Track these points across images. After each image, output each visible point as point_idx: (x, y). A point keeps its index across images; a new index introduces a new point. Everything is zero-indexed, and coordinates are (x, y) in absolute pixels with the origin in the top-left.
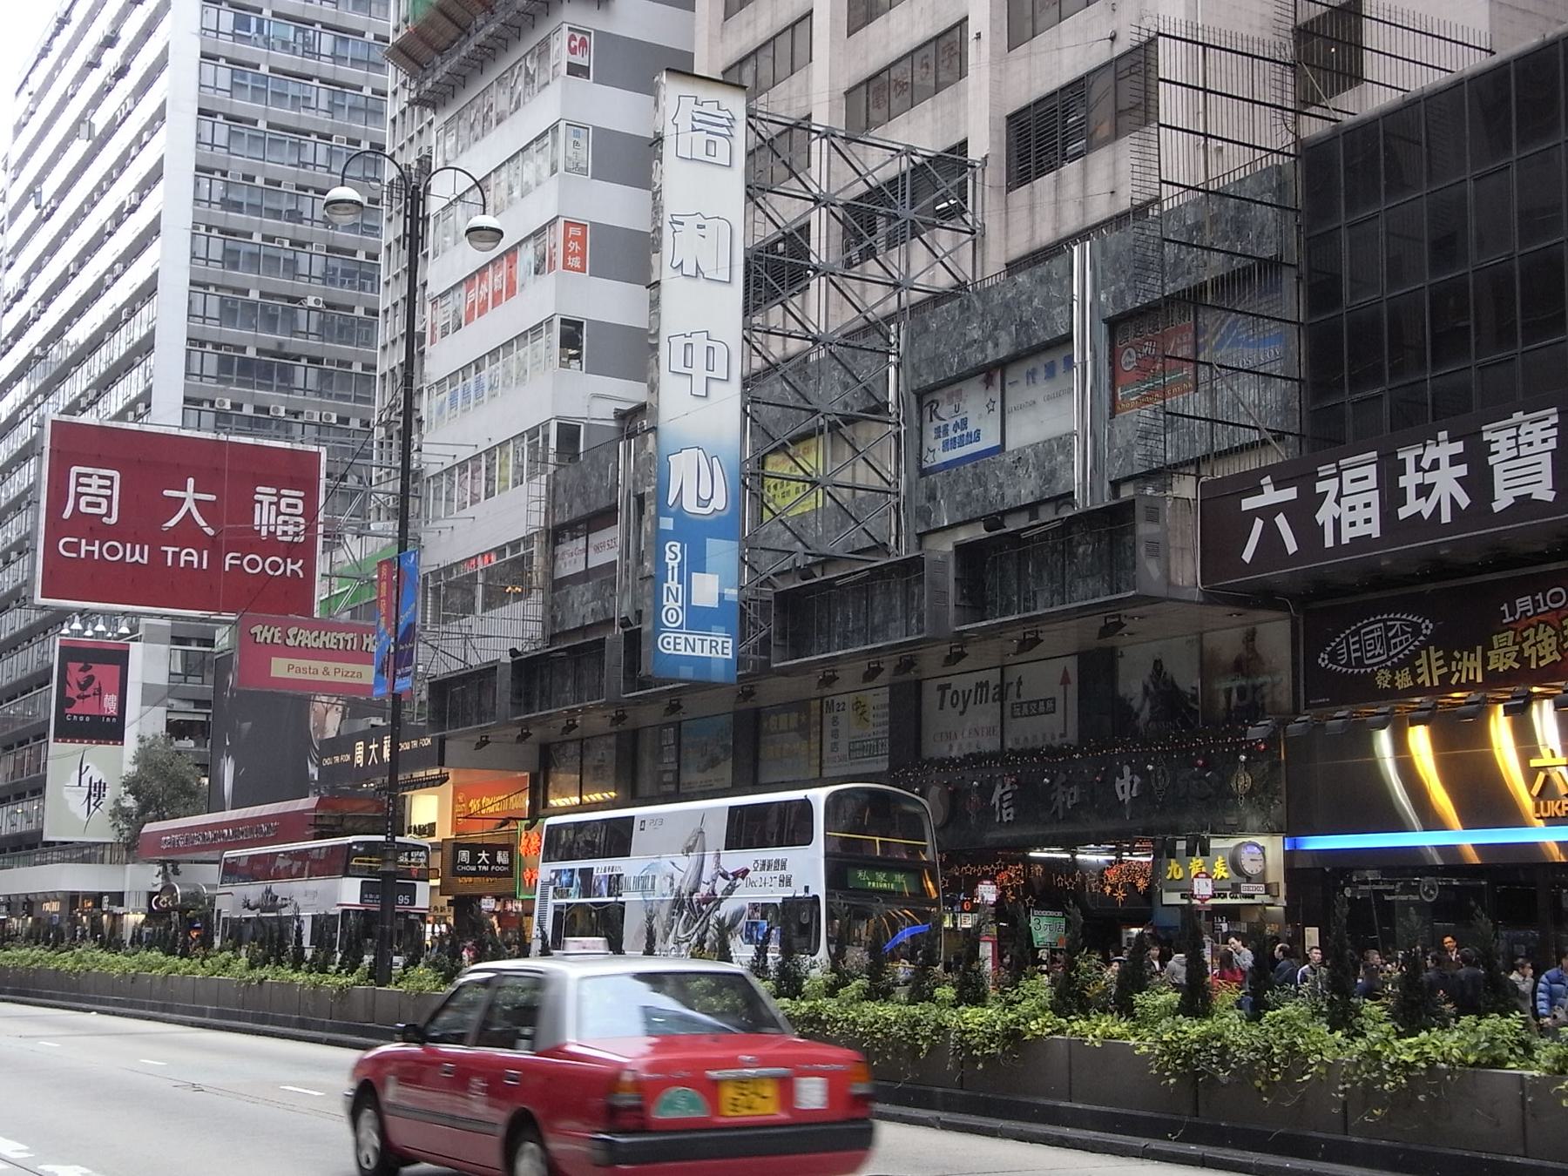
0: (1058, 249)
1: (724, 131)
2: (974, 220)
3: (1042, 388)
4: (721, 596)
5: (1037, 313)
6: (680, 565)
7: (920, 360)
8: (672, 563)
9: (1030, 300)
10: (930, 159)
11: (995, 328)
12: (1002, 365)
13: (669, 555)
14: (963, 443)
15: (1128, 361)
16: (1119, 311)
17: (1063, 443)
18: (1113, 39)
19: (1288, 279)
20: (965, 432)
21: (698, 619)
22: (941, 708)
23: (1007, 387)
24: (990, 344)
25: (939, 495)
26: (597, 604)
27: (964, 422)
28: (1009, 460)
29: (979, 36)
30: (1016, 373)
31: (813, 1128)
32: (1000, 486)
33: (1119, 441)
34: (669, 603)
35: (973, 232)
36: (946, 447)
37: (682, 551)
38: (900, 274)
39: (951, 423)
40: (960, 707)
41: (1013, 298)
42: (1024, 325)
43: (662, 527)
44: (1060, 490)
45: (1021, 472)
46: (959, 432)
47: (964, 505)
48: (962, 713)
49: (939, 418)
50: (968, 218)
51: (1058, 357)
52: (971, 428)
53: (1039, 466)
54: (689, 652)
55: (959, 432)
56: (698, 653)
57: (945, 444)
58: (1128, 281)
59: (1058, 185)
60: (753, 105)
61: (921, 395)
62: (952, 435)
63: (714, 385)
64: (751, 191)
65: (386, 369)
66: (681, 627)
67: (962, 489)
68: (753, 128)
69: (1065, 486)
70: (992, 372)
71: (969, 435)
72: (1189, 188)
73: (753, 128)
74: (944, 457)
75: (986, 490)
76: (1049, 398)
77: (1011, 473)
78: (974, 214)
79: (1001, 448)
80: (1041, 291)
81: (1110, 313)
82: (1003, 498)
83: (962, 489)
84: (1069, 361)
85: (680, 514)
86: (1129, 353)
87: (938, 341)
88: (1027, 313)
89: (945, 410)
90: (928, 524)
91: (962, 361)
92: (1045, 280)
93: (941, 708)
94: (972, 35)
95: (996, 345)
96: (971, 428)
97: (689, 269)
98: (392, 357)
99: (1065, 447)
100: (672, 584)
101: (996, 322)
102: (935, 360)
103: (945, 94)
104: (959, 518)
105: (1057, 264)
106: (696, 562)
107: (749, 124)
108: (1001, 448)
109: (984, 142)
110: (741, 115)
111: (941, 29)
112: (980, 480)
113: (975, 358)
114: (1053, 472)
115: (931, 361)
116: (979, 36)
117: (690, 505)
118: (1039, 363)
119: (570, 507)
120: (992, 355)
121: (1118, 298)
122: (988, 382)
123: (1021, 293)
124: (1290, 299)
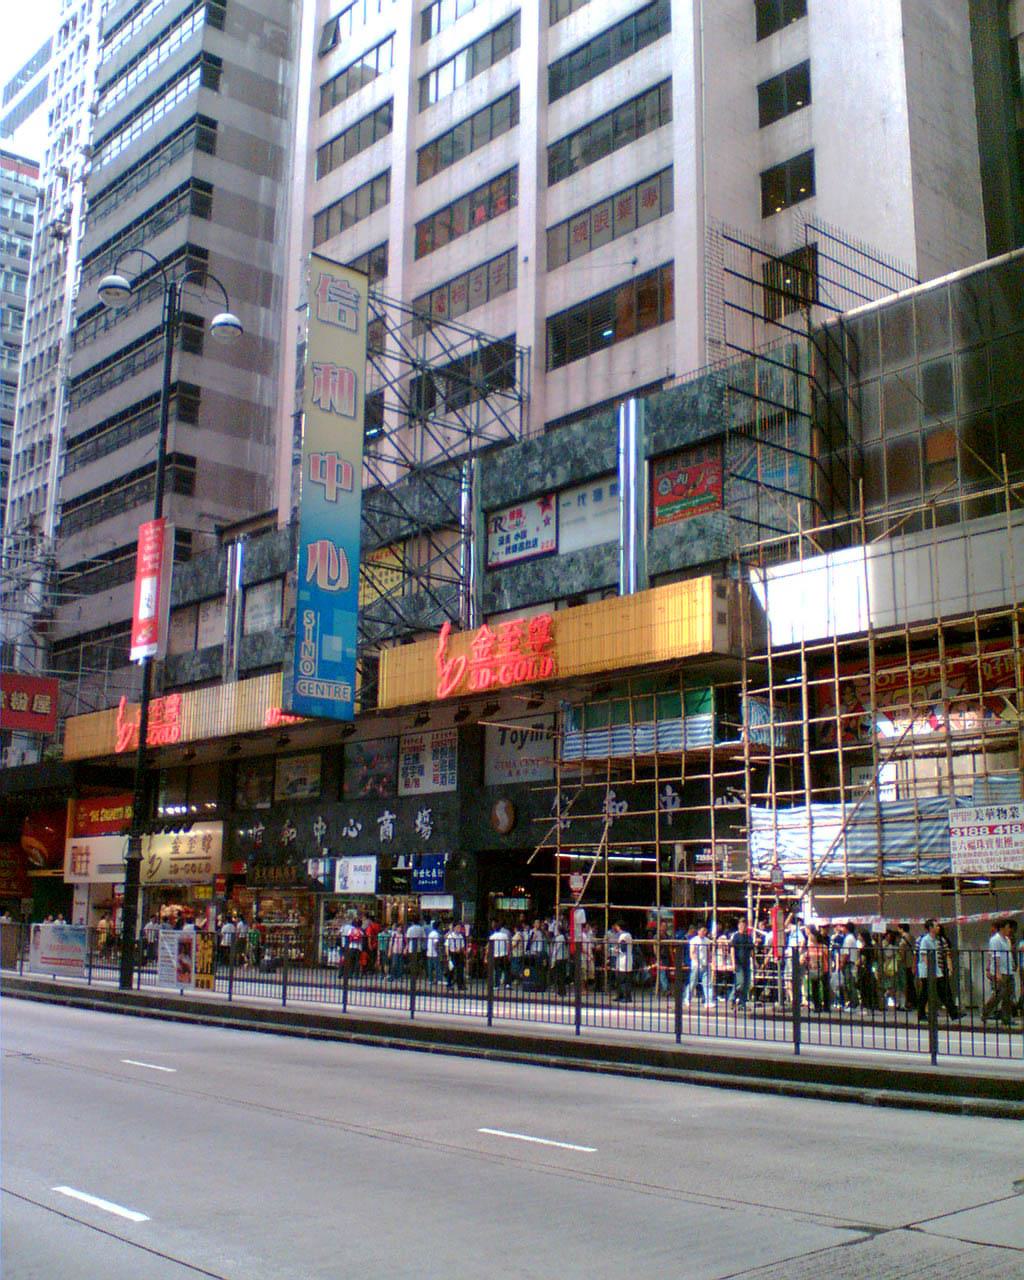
0: (610, 405)
1: (352, 304)
2: (522, 389)
3: (591, 506)
4: (344, 653)
5: (589, 452)
6: (315, 629)
7: (489, 487)
8: (309, 626)
9: (584, 442)
10: (493, 344)
11: (554, 464)
12: (558, 491)
13: (306, 620)
14: (522, 547)
15: (664, 488)
16: (658, 451)
17: (611, 548)
18: (634, 263)
19: (804, 425)
20: (524, 541)
21: (327, 670)
22: (502, 743)
23: (561, 508)
24: (549, 475)
25: (502, 588)
26: (205, 666)
27: (524, 534)
28: (563, 561)
29: (526, 260)
30: (569, 498)
31: (528, 1056)
32: (555, 579)
33: (658, 547)
34: (305, 656)
35: (520, 399)
36: (508, 550)
37: (316, 617)
38: (471, 423)
39: (513, 534)
40: (519, 743)
41: (569, 442)
42: (578, 462)
43: (301, 598)
44: (607, 581)
45: (572, 569)
46: (520, 541)
47: (524, 594)
48: (520, 748)
49: (501, 529)
50: (518, 389)
51: (605, 486)
52: (530, 537)
53: (590, 566)
54: (319, 696)
55: (520, 541)
56: (326, 696)
57: (508, 550)
58: (666, 429)
59: (588, 366)
60: (372, 288)
61: (487, 512)
62: (513, 542)
63: (342, 495)
64: (371, 354)
65: (16, 496)
66: (313, 676)
67: (522, 582)
68: (373, 308)
69: (611, 579)
70: (545, 497)
71: (528, 543)
72: (743, 351)
73: (373, 308)
74: (504, 558)
75: (543, 582)
76: (596, 515)
77: (564, 570)
78: (521, 384)
79: (554, 552)
80: (593, 436)
81: (652, 451)
82: (558, 588)
83: (522, 582)
84: (614, 489)
85: (313, 587)
86: (666, 483)
87: (504, 473)
88: (581, 451)
89: (507, 524)
90: (493, 607)
91: (524, 488)
92: (597, 428)
93: (502, 743)
94: (520, 257)
95: (554, 476)
96: (530, 537)
97: (325, 405)
98: (20, 488)
99: (610, 551)
100: (308, 642)
101: (553, 459)
102: (502, 488)
103: (495, 303)
104: (520, 602)
105: (604, 419)
106: (327, 628)
107: (369, 304)
108: (554, 552)
109: (528, 337)
110: (364, 294)
111: (492, 256)
112: (538, 575)
113: (535, 485)
114: (601, 569)
115: (497, 489)
116: (526, 260)
117: (322, 583)
118: (589, 490)
119: (184, 593)
120: (549, 482)
121: (657, 441)
122: (545, 505)
123: (575, 438)
124: (804, 438)
